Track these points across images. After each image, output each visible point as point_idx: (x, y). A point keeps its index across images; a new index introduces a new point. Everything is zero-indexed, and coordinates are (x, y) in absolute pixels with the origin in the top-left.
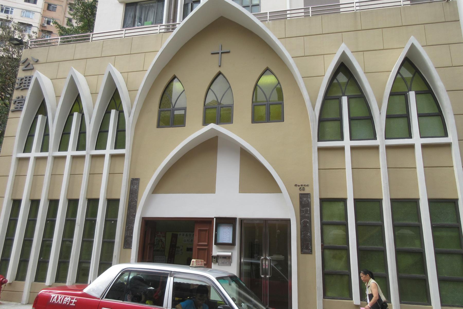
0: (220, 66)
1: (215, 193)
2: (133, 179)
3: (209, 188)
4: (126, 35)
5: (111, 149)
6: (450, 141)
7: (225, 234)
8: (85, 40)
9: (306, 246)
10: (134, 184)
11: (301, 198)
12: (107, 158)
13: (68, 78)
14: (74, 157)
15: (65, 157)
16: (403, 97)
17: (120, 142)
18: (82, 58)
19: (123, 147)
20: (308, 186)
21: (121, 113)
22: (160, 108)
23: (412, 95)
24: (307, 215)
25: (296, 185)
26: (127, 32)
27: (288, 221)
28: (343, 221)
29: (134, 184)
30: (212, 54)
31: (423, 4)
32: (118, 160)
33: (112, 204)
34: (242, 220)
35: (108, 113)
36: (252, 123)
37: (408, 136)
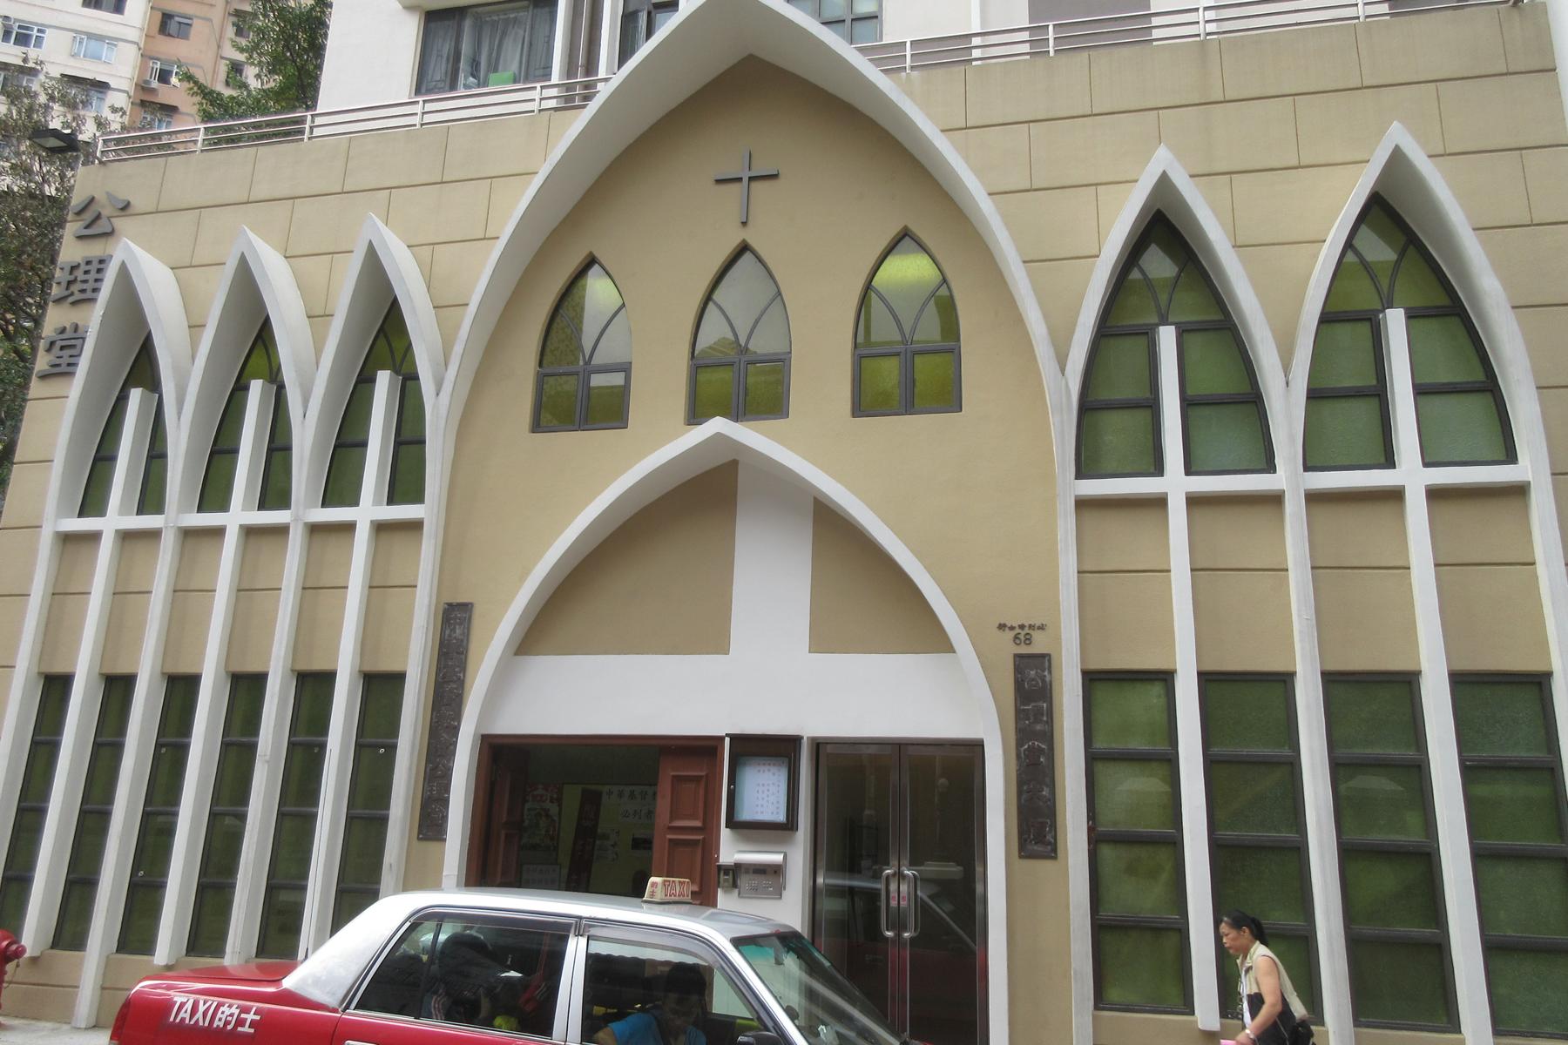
0: (744, 224)
1: (727, 652)
2: (450, 605)
3: (709, 634)
4: (428, 118)
5: (376, 503)
6: (1525, 478)
7: (763, 792)
8: (287, 134)
9: (1036, 832)
10: (455, 623)
11: (1018, 670)
12: (362, 535)
13: (232, 265)
14: (250, 533)
15: (219, 532)
16: (1364, 329)
17: (405, 481)
18: (277, 195)
19: (417, 496)
20: (1042, 628)
21: (408, 381)
22: (540, 365)
23: (1395, 321)
24: (1038, 727)
25: (1002, 627)
26: (429, 107)
27: (975, 749)
28: (1163, 747)
29: (455, 623)
30: (718, 181)
31: (1434, 14)
32: (398, 542)
33: (381, 689)
34: (818, 745)
35: (365, 381)
36: (854, 415)
37: (1382, 460)
